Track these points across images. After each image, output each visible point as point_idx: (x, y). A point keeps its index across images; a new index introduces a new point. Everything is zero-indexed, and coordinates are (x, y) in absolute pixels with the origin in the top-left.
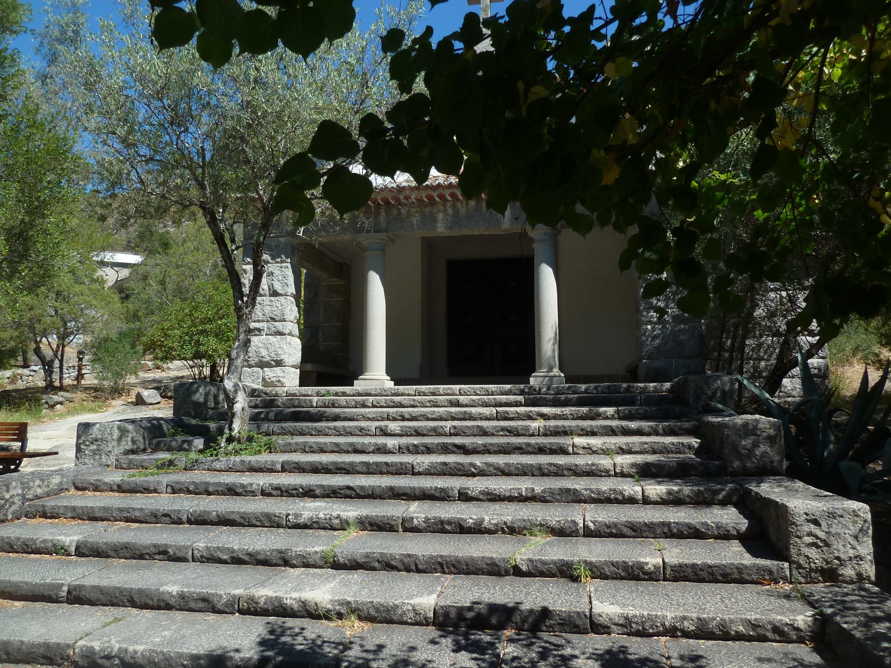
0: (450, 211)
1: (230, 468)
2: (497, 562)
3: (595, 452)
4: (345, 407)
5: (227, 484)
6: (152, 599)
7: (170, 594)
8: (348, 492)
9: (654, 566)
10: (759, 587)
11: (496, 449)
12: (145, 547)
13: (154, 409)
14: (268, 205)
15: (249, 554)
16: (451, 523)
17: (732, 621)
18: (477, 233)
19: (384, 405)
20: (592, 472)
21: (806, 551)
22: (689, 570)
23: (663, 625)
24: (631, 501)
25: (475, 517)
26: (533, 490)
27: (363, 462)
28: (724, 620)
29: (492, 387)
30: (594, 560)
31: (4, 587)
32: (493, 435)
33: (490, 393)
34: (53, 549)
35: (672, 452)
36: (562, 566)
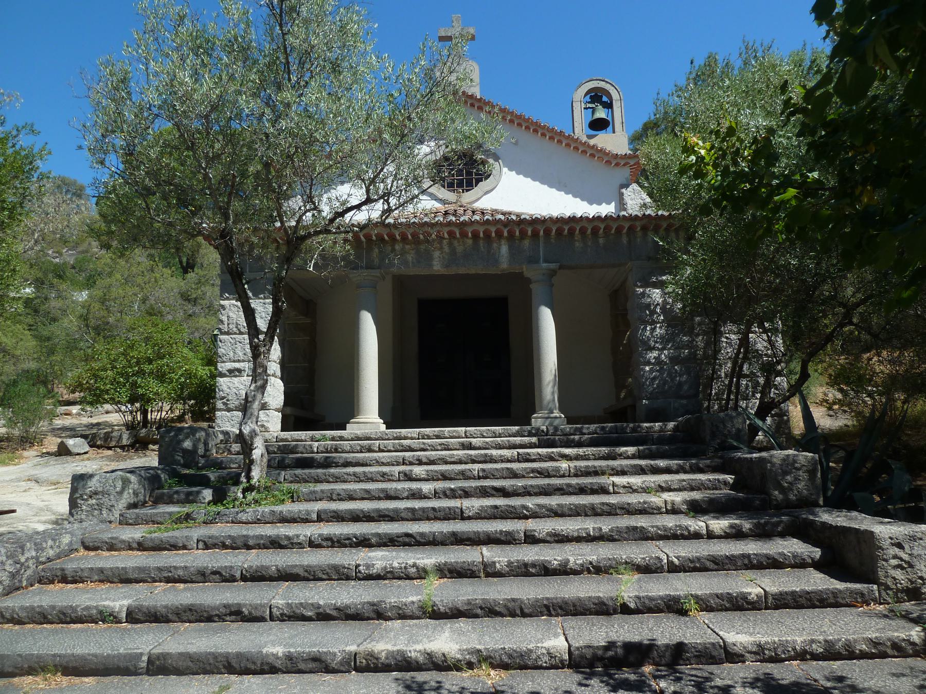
0: (446, 249)
1: (258, 520)
2: (605, 601)
3: (635, 491)
4: (349, 452)
5: (270, 537)
6: (254, 663)
7: (276, 656)
8: (407, 540)
9: (757, 596)
10: (853, 610)
11: (536, 490)
12: (213, 608)
13: (83, 460)
14: (292, 238)
15: (338, 609)
16: (535, 565)
17: (855, 641)
18: (473, 272)
19: (392, 449)
20: (645, 510)
21: (892, 572)
22: (789, 597)
23: (794, 649)
24: (697, 536)
25: (559, 558)
26: (600, 529)
27: (408, 509)
28: (849, 640)
29: (499, 429)
30: (699, 593)
31: (67, 662)
32: (523, 477)
33: (497, 435)
34: (99, 616)
35: (709, 489)
36: (669, 601)
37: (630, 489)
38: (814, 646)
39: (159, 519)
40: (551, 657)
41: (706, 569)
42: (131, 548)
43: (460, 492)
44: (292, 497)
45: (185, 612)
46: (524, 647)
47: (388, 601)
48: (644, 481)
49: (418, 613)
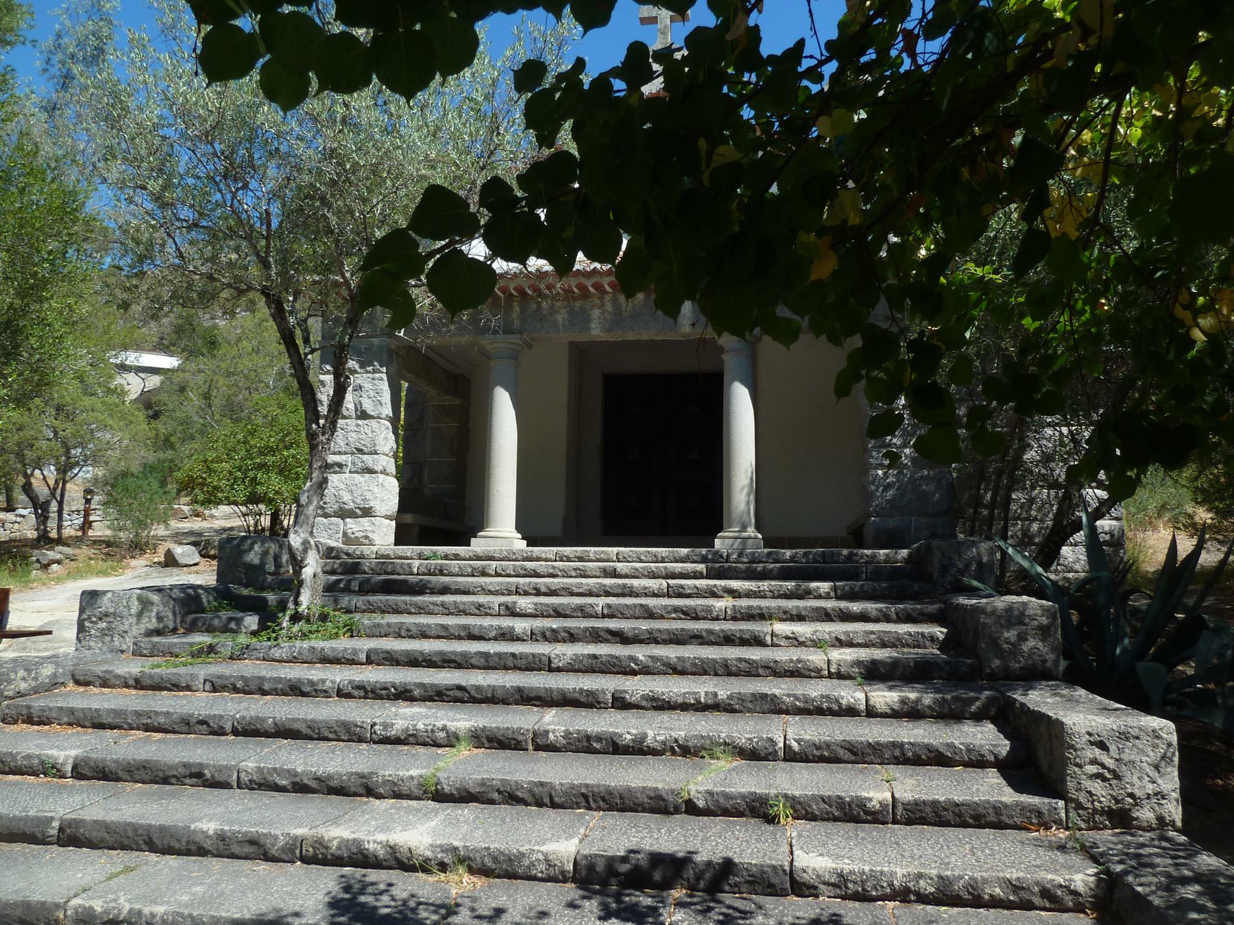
1: (295, 657)
2: (664, 794)
4: (458, 575)
5: (290, 680)
6: (178, 840)
7: (204, 833)
8: (459, 694)
9: (880, 803)
12: (175, 767)
17: (985, 881)
18: (646, 338)
19: (512, 573)
20: (798, 671)
22: (928, 810)
23: (891, 885)
25: (634, 731)
26: (715, 695)
27: (481, 653)
28: (975, 879)
29: (662, 551)
30: (797, 793)
32: (662, 617)
33: (660, 559)
35: (909, 646)
36: (753, 801)
37: (796, 641)
38: (922, 883)
39: (177, 650)
40: (550, 865)
41: (838, 760)
42: (127, 686)
43: (563, 634)
44: (351, 630)
45: (138, 769)
46: (514, 848)
47: (381, 773)
48: (816, 631)
49: (416, 792)
